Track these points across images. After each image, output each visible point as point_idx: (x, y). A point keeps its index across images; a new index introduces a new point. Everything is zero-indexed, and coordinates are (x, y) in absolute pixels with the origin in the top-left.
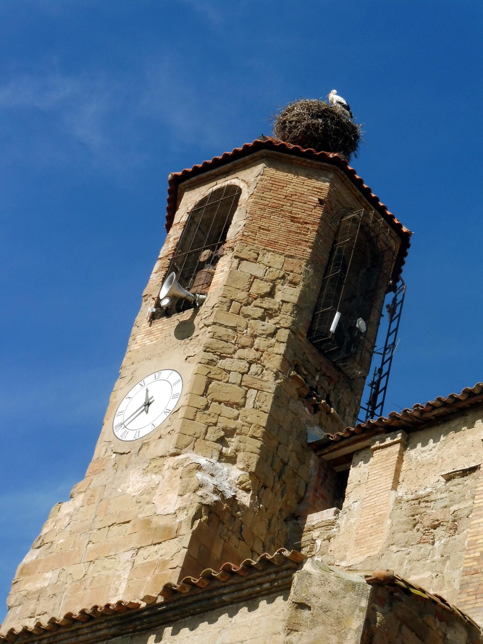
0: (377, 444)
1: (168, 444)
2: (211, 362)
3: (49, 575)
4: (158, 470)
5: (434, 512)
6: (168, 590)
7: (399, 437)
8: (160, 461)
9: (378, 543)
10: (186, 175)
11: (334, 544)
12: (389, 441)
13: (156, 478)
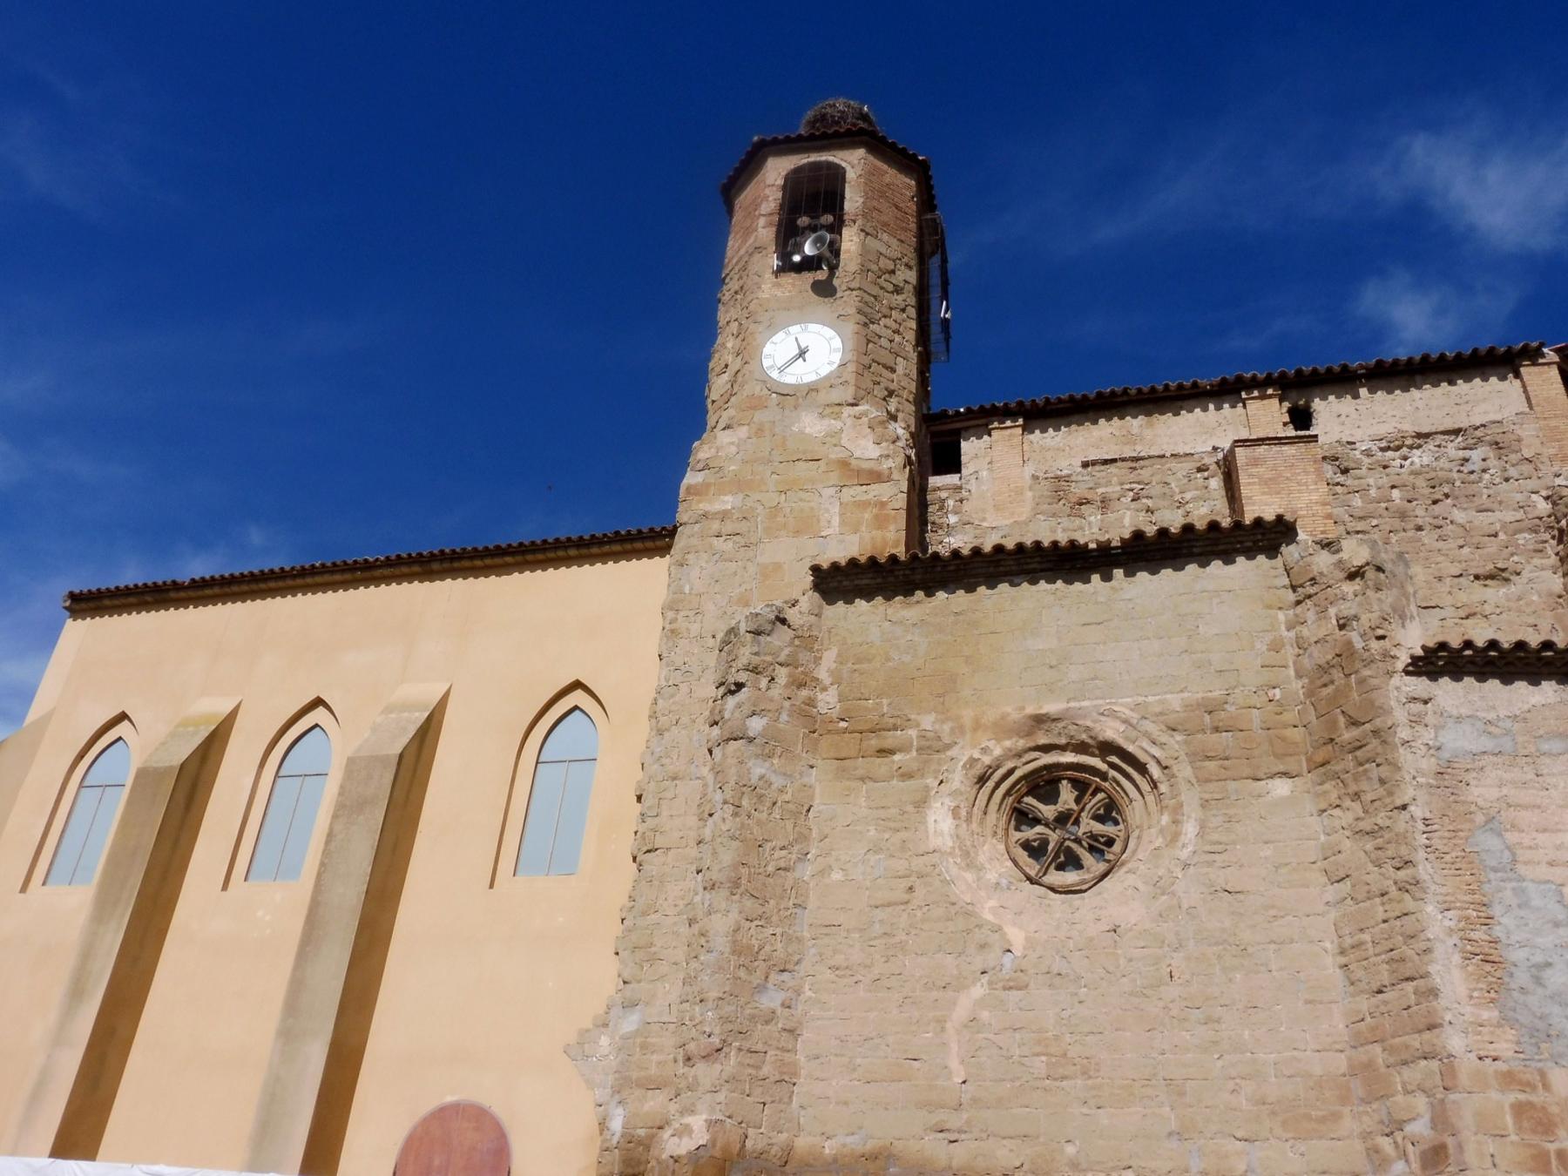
0: (996, 424)
1: (848, 394)
2: (865, 325)
3: (729, 498)
4: (838, 416)
5: (1078, 491)
6: (1055, 544)
7: (1021, 421)
8: (837, 409)
9: (1024, 512)
10: (775, 141)
11: (966, 506)
12: (1008, 423)
13: (837, 424)
